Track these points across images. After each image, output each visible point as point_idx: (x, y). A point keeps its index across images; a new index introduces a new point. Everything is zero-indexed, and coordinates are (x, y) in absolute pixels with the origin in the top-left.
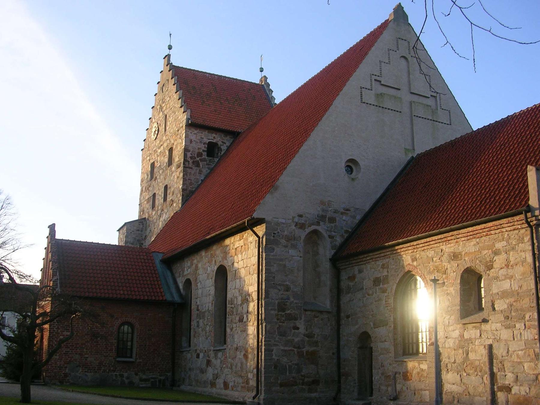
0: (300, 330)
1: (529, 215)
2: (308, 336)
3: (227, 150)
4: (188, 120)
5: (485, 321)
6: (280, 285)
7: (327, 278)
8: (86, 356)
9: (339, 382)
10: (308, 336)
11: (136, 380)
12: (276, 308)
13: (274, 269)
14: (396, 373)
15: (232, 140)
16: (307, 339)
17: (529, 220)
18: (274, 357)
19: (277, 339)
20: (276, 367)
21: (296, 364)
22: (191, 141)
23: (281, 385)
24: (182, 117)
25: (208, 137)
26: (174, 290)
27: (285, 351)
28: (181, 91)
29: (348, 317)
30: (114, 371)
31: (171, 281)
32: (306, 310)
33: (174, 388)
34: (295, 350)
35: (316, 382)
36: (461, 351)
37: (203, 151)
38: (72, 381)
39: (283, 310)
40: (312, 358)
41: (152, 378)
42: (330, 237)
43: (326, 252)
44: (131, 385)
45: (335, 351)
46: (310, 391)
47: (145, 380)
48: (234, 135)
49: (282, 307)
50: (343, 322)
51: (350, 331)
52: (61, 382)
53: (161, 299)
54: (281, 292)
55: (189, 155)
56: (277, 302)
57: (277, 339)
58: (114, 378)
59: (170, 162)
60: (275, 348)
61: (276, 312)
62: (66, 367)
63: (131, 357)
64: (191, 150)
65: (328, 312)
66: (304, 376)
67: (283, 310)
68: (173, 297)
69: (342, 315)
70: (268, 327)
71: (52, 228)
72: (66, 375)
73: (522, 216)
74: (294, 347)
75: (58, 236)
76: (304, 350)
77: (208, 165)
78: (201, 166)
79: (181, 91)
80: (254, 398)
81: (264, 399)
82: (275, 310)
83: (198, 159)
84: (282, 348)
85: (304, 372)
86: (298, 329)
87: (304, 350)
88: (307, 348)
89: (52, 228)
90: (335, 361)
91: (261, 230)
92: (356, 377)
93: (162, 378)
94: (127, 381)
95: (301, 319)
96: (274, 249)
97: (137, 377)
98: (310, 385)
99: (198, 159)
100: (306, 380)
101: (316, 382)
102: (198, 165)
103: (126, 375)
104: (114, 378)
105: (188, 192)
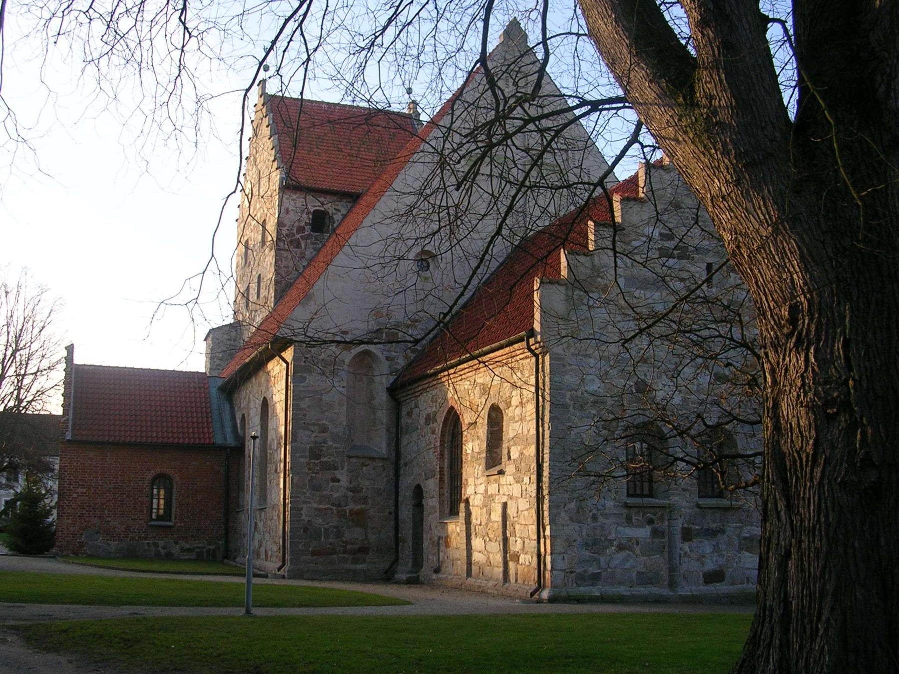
0: (341, 483)
1: (532, 341)
2: (353, 490)
3: (342, 221)
4: (281, 179)
5: (501, 472)
6: (314, 425)
7: (383, 416)
8: (109, 519)
9: (397, 551)
10: (353, 490)
11: (175, 550)
12: (307, 454)
13: (304, 404)
14: (439, 538)
15: (350, 205)
16: (351, 494)
17: (533, 348)
18: (303, 517)
19: (308, 495)
20: (306, 530)
21: (334, 527)
22: (287, 211)
23: (314, 553)
24: (276, 177)
25: (314, 204)
26: (228, 430)
27: (320, 509)
28: (276, 136)
29: (406, 465)
30: (146, 538)
31: (227, 417)
32: (350, 457)
33: (225, 561)
34: (334, 508)
35: (364, 550)
36: (484, 510)
37: (306, 223)
38: (89, 553)
39: (318, 457)
40: (359, 518)
41: (199, 548)
42: (387, 358)
43: (383, 380)
44: (169, 557)
45: (392, 509)
46: (355, 561)
47: (189, 550)
48: (353, 198)
49: (315, 453)
50: (402, 472)
51: (407, 482)
52: (76, 554)
53: (207, 441)
54: (315, 434)
55: (285, 231)
56: (308, 447)
57: (308, 495)
58: (146, 548)
59: (263, 242)
60: (304, 506)
61: (308, 460)
62: (82, 534)
63: (170, 520)
64: (288, 223)
65: (383, 459)
66: (346, 542)
67: (318, 457)
68: (225, 439)
69: (402, 462)
70: (295, 480)
71: (70, 349)
72: (82, 544)
73: (524, 344)
74: (333, 505)
75: (78, 360)
76: (347, 508)
77: (314, 244)
78: (303, 246)
79: (276, 136)
80: (279, 569)
81: (288, 571)
82: (306, 457)
83: (298, 236)
84: (315, 506)
85: (347, 536)
86: (338, 481)
87: (347, 508)
88: (352, 506)
89: (70, 349)
90: (392, 523)
91: (289, 354)
92: (410, 544)
93: (212, 547)
94: (163, 552)
95: (343, 468)
96: (305, 378)
97: (178, 547)
98: (354, 554)
99: (298, 236)
100: (349, 547)
101: (364, 550)
102: (298, 246)
103: (161, 543)
104: (146, 548)
105: (283, 285)
